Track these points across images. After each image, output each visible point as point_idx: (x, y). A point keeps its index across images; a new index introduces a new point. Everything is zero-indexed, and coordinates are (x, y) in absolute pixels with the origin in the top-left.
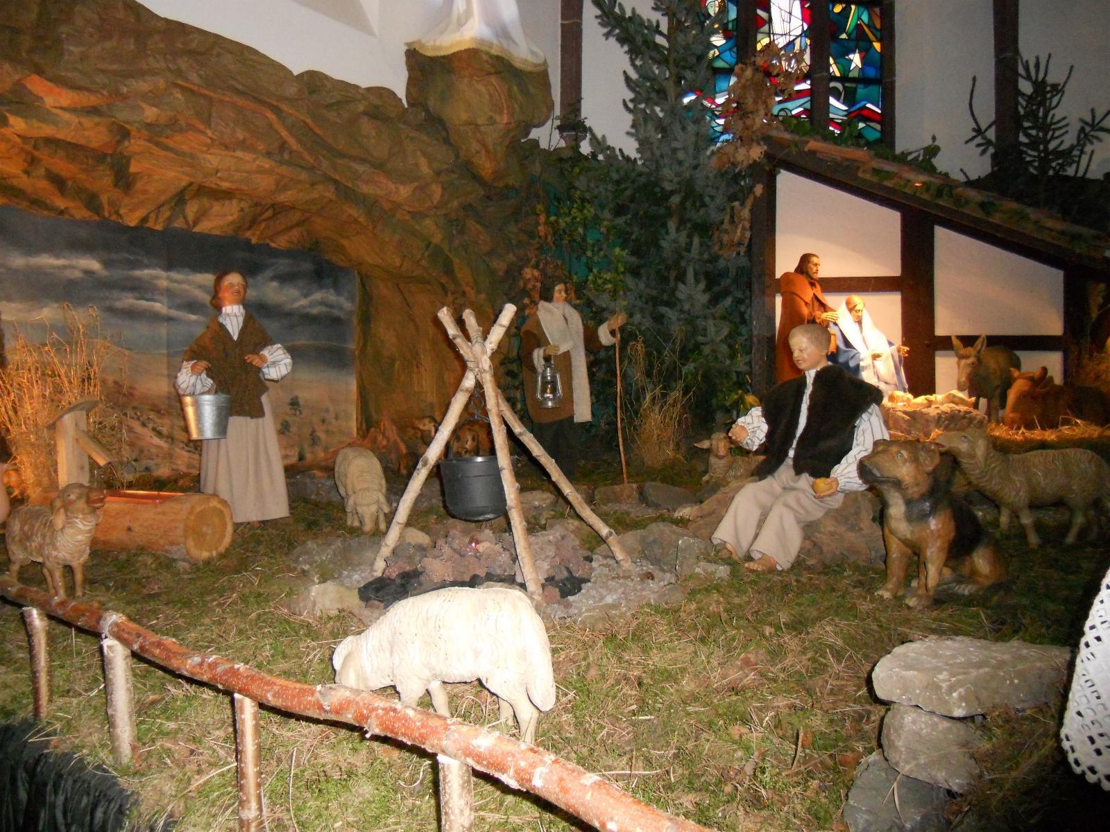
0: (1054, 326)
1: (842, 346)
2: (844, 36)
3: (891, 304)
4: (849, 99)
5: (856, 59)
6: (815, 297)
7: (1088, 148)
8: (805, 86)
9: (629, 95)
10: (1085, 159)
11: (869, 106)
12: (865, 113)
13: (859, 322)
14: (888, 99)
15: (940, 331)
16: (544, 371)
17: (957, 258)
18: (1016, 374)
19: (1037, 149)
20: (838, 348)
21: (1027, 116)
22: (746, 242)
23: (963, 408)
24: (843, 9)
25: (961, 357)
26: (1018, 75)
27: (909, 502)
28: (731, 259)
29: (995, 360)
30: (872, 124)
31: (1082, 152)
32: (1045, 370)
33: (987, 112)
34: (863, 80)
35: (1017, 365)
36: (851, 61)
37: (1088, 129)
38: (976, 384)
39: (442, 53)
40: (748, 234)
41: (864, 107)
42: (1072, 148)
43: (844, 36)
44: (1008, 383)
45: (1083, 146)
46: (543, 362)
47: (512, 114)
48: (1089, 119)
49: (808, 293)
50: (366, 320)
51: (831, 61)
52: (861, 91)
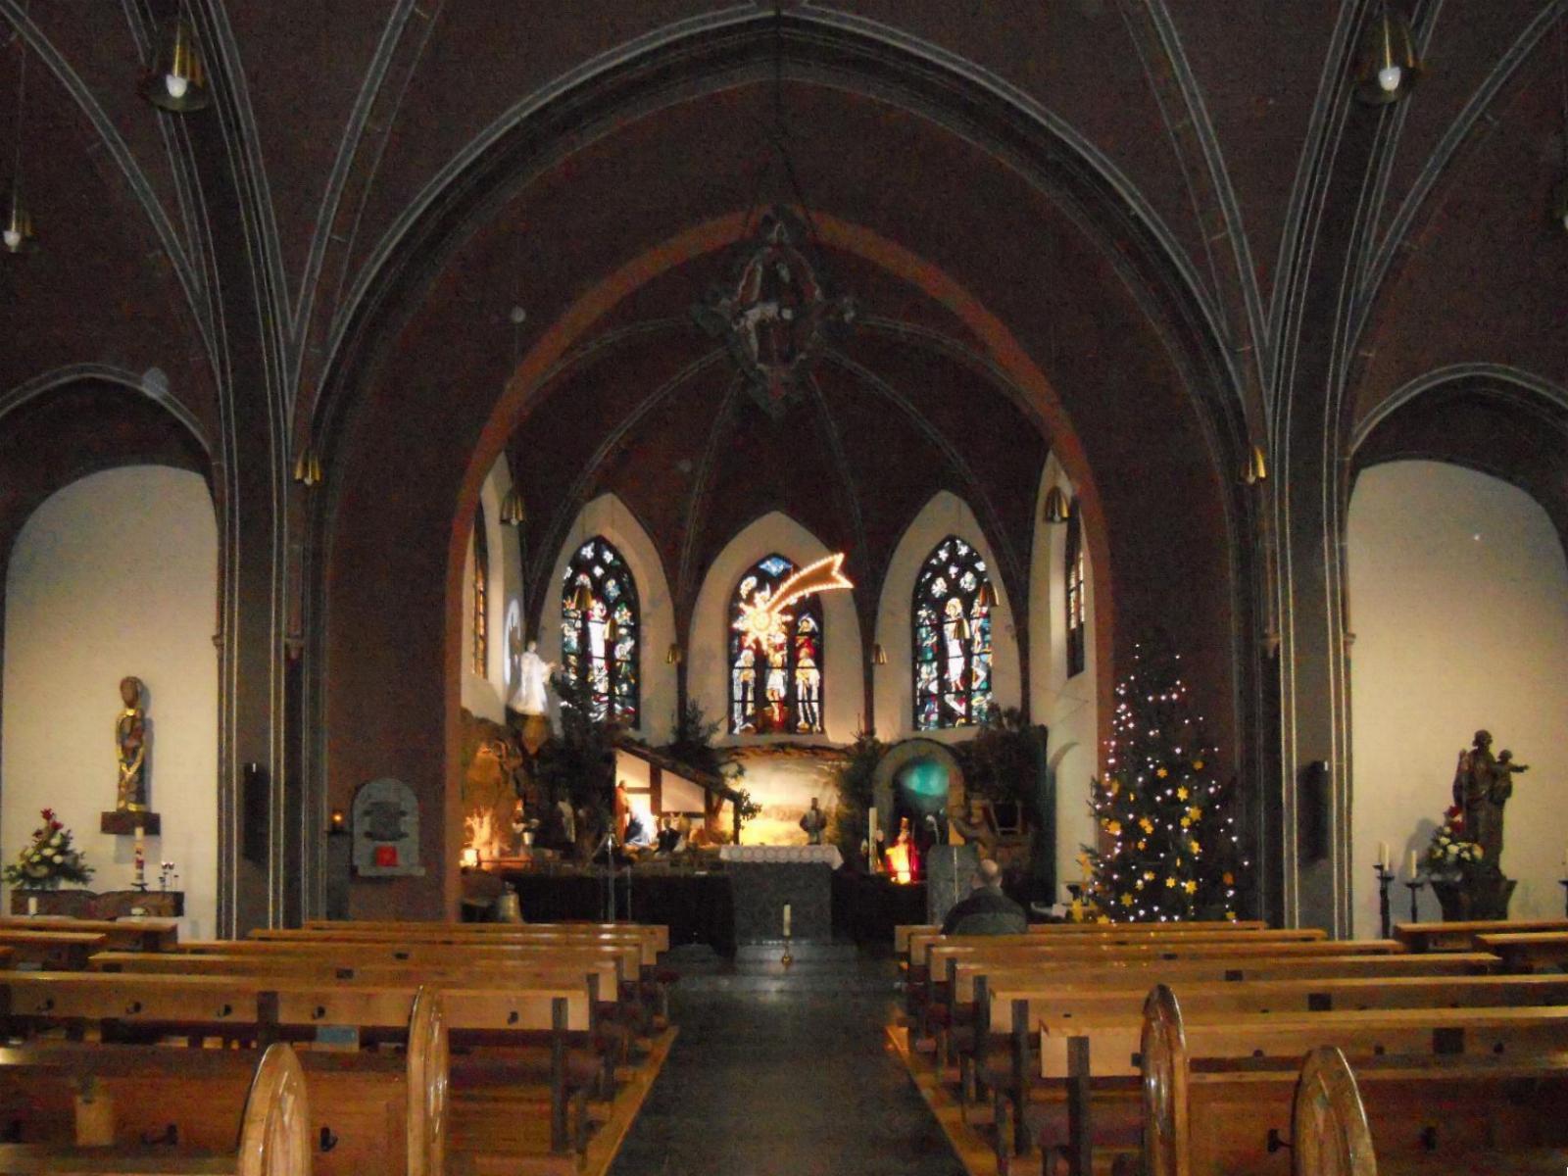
0: (701, 808)
14: (637, 705)
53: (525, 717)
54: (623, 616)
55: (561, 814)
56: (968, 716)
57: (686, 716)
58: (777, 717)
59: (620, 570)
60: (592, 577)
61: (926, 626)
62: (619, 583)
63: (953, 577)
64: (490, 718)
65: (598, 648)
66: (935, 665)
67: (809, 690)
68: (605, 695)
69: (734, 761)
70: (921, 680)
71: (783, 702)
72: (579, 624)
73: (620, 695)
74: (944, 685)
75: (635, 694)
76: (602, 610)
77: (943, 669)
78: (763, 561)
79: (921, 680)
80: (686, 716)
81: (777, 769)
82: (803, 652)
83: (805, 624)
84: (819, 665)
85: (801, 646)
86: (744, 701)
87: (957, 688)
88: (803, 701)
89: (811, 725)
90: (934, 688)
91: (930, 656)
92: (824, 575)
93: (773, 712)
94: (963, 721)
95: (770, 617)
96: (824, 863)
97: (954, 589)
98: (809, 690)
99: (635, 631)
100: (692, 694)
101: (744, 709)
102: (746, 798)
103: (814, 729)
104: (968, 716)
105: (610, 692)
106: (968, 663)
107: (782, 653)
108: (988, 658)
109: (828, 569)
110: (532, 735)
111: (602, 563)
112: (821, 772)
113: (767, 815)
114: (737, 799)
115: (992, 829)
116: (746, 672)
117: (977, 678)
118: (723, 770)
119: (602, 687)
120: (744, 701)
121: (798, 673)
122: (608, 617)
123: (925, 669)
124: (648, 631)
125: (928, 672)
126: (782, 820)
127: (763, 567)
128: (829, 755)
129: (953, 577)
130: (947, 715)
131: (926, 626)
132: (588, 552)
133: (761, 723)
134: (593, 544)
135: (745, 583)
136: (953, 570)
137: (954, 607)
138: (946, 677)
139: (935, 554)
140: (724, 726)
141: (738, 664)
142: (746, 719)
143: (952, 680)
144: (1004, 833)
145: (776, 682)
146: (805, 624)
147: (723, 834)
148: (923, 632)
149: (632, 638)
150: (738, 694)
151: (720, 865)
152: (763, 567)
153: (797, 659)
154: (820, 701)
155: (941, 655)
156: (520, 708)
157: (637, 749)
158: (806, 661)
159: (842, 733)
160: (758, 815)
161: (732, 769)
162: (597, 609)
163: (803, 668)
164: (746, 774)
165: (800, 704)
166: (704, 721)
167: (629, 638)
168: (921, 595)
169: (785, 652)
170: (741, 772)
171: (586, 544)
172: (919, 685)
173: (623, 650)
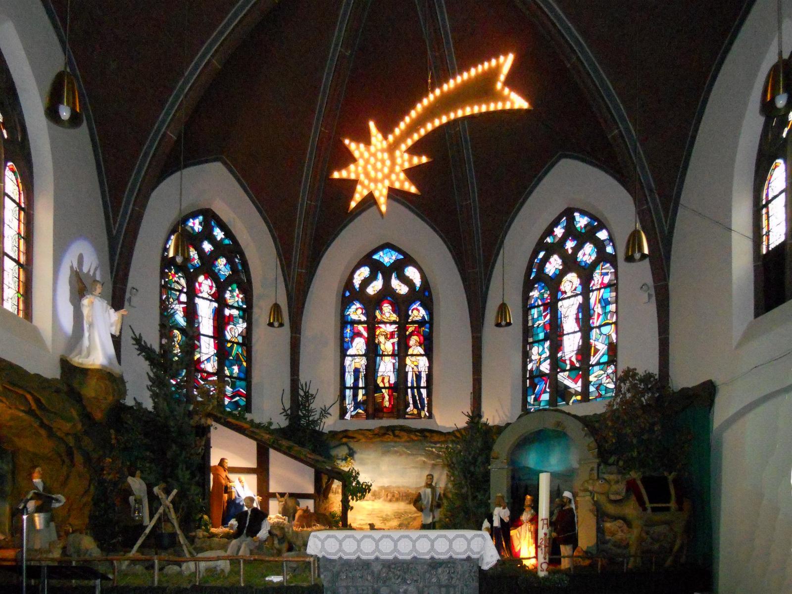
0: (311, 490)
1: (237, 497)
2: (231, 358)
3: (253, 479)
4: (233, 386)
5: (236, 369)
6: (226, 476)
7: (324, 420)
8: (215, 378)
9: (150, 383)
10: (322, 424)
11: (241, 390)
12: (239, 393)
13: (243, 487)
14: (249, 388)
15: (271, 491)
16: (135, 506)
17: (278, 463)
18: (298, 508)
19: (305, 419)
20: (236, 497)
21: (302, 404)
22: (202, 454)
23: (281, 520)
24: (231, 346)
25: (280, 502)
26: (299, 388)
27: (279, 540)
28: (197, 460)
29: (291, 502)
30: (243, 398)
31: (321, 421)
32: (307, 507)
33: (288, 405)
34: (238, 378)
35: (298, 504)
36: (233, 369)
37: (323, 412)
38: (284, 512)
39: (84, 367)
40: (203, 451)
41: (239, 390)
42: (318, 419)
43: (231, 358)
44: (295, 511)
45: (322, 419)
46: (134, 502)
47: (114, 396)
48: (324, 408)
49: (224, 474)
50: (13, 473)
51: (226, 368)
52: (238, 383)
53: (84, 372)
54: (234, 297)
55: (129, 492)
56: (585, 394)
57: (299, 400)
58: (387, 404)
59: (232, 250)
60: (201, 252)
61: (538, 306)
62: (230, 262)
63: (570, 251)
64: (41, 373)
65: (206, 326)
66: (547, 344)
67: (418, 377)
69: (345, 444)
70: (531, 361)
71: (392, 388)
72: (183, 298)
74: (557, 364)
75: (247, 376)
76: (211, 288)
77: (556, 346)
78: (375, 251)
79: (531, 361)
80: (299, 400)
81: (386, 452)
82: (414, 340)
83: (415, 312)
84: (429, 353)
85: (412, 334)
86: (355, 388)
87: (572, 363)
88: (412, 388)
89: (419, 411)
90: (545, 367)
91: (541, 336)
92: (483, 89)
93: (383, 398)
94: (579, 398)
95: (393, 158)
96: (469, 559)
97: (570, 264)
98: (418, 377)
100: (303, 378)
101: (355, 396)
102: (356, 478)
103: (423, 414)
104: (585, 394)
105: (220, 372)
106: (586, 338)
107: (392, 341)
108: (609, 330)
109: (491, 77)
110: (93, 394)
111: (212, 240)
112: (430, 455)
113: (376, 496)
114: (347, 479)
115: (641, 503)
116: (357, 359)
117: (596, 351)
118: (334, 452)
119: (210, 367)
120: (355, 388)
121: (408, 360)
122: (218, 297)
123: (535, 350)
124: (261, 314)
125: (539, 353)
126: (390, 501)
127: (376, 257)
128: (436, 438)
129: (570, 251)
130: (560, 393)
131: (538, 306)
132: (196, 225)
133: (373, 409)
134: (201, 218)
135: (358, 272)
136: (570, 245)
137: (571, 282)
138: (559, 355)
139: (550, 232)
140: (335, 411)
142: (357, 405)
143: (567, 357)
144: (654, 510)
145: (386, 369)
146: (415, 312)
147: (333, 515)
148: (535, 312)
149: (244, 320)
150: (349, 380)
151: (306, 565)
152: (376, 257)
153: (408, 347)
154: (429, 387)
155: (555, 334)
156: (78, 360)
157: (239, 422)
158: (415, 348)
159: (450, 416)
160: (368, 495)
161: (343, 451)
162: (205, 285)
163: (412, 355)
164: (356, 456)
165: (409, 390)
166: (316, 406)
167: (241, 321)
168: (534, 276)
169: (396, 340)
170: (351, 454)
171: (194, 215)
172: (529, 367)
173: (235, 331)
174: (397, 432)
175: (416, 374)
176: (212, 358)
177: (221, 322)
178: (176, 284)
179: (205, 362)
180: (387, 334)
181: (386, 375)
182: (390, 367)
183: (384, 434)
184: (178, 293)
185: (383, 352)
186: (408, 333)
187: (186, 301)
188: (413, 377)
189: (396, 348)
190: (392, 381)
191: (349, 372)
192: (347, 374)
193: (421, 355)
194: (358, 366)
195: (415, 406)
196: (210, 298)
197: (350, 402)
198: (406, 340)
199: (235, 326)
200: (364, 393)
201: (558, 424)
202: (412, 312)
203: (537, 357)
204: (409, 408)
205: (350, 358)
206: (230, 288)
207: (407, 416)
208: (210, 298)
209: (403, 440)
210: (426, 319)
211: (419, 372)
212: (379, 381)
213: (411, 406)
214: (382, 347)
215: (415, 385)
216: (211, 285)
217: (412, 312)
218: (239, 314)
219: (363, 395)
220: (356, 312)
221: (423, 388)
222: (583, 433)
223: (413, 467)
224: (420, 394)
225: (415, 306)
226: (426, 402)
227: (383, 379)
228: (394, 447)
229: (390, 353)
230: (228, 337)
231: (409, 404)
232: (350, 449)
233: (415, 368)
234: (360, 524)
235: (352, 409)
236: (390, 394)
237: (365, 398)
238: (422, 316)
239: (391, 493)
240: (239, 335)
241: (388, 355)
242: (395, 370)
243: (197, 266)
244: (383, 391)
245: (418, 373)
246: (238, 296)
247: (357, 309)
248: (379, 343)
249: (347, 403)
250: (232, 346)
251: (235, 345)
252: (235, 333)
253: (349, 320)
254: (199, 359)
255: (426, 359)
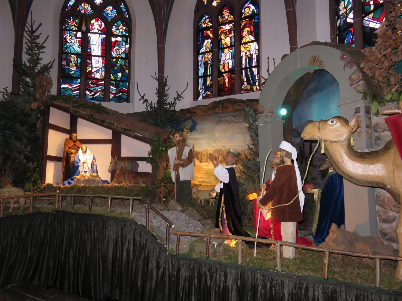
4: (117, 86)
5: (120, 75)
24: (116, 60)
41: (122, 89)
43: (116, 68)
67: (250, 59)
68: (101, 80)
71: (231, 72)
73: (115, 80)
81: (219, 122)
84: (257, 39)
85: (245, 27)
88: (246, 68)
89: (252, 86)
93: (225, 80)
98: (250, 59)
99: (128, 38)
101: (205, 82)
103: (255, 88)
105: (106, 78)
122: (107, 32)
141: (202, 51)
142: (206, 88)
145: (227, 57)
146: (247, 10)
149: (126, 42)
150: (201, 72)
163: (245, 43)
164: (198, 127)
165: (243, 71)
167: (124, 44)
174: (225, 105)
175: (248, 57)
176: (100, 70)
177: (107, 46)
178: (73, 27)
179: (95, 73)
180: (227, 32)
181: (226, 62)
182: (229, 56)
183: (215, 108)
184: (75, 32)
185: (224, 45)
186: (241, 27)
187: (81, 36)
188: (246, 60)
189: (233, 40)
190: (231, 65)
191: (201, 65)
192: (199, 67)
193: (252, 41)
194: (207, 60)
195: (248, 83)
196: (100, 32)
197: (202, 88)
198: (241, 31)
199: (120, 47)
200: (211, 79)
201: (315, 60)
202: (244, 10)
203: (344, 11)
204: (244, 85)
205: (201, 56)
206: (116, 24)
207: (242, 92)
208: (100, 32)
209: (229, 110)
210: (256, 12)
211: (251, 55)
212: (221, 68)
213: (245, 83)
214: (223, 42)
215: (248, 66)
216: (100, 24)
217: (244, 10)
218: (122, 40)
219: (210, 81)
220: (206, 23)
221: (255, 67)
222: (343, 63)
223: (240, 133)
224: (252, 73)
225: (247, 5)
226: (257, 78)
227: (224, 65)
228: (226, 117)
229: (229, 45)
230: (114, 55)
231: (244, 81)
232: (194, 122)
233: (248, 53)
234: (199, 182)
235: (203, 92)
236: (229, 76)
237: (211, 82)
238: (252, 10)
239: (222, 156)
240: (122, 53)
241: (227, 47)
242: (233, 57)
243: (90, 14)
244: (224, 75)
245: (250, 56)
246: (122, 28)
247: (206, 19)
248: (222, 39)
249: (200, 88)
250: (117, 62)
251: (119, 60)
252: (119, 52)
253: (201, 28)
254: (91, 71)
255: (256, 43)
